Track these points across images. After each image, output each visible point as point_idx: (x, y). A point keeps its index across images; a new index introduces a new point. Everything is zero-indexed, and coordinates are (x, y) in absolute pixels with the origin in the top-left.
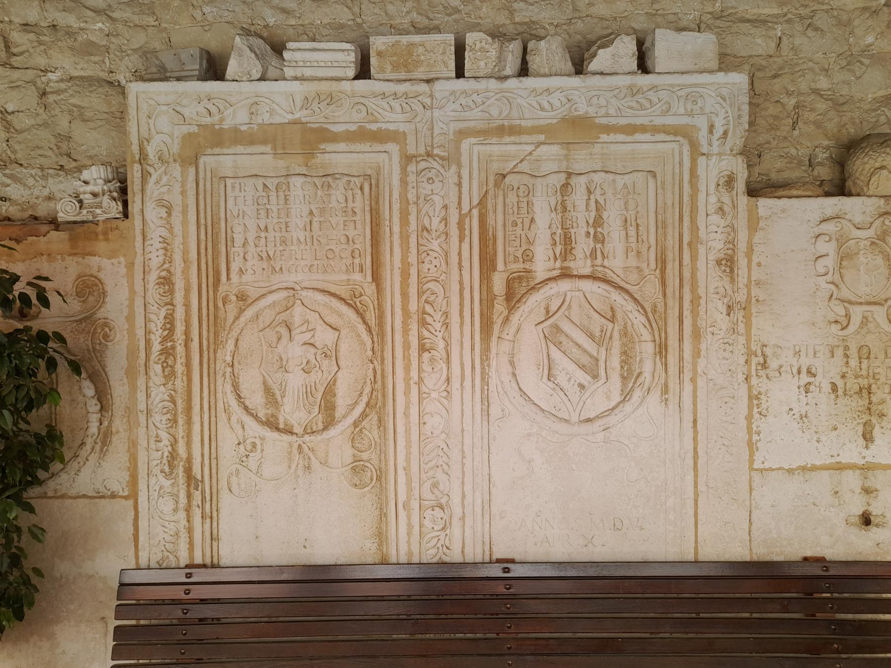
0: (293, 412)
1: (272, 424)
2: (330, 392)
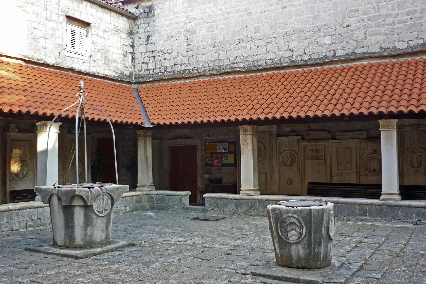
0: (415, 164)
1: (411, 166)
2: (421, 162)
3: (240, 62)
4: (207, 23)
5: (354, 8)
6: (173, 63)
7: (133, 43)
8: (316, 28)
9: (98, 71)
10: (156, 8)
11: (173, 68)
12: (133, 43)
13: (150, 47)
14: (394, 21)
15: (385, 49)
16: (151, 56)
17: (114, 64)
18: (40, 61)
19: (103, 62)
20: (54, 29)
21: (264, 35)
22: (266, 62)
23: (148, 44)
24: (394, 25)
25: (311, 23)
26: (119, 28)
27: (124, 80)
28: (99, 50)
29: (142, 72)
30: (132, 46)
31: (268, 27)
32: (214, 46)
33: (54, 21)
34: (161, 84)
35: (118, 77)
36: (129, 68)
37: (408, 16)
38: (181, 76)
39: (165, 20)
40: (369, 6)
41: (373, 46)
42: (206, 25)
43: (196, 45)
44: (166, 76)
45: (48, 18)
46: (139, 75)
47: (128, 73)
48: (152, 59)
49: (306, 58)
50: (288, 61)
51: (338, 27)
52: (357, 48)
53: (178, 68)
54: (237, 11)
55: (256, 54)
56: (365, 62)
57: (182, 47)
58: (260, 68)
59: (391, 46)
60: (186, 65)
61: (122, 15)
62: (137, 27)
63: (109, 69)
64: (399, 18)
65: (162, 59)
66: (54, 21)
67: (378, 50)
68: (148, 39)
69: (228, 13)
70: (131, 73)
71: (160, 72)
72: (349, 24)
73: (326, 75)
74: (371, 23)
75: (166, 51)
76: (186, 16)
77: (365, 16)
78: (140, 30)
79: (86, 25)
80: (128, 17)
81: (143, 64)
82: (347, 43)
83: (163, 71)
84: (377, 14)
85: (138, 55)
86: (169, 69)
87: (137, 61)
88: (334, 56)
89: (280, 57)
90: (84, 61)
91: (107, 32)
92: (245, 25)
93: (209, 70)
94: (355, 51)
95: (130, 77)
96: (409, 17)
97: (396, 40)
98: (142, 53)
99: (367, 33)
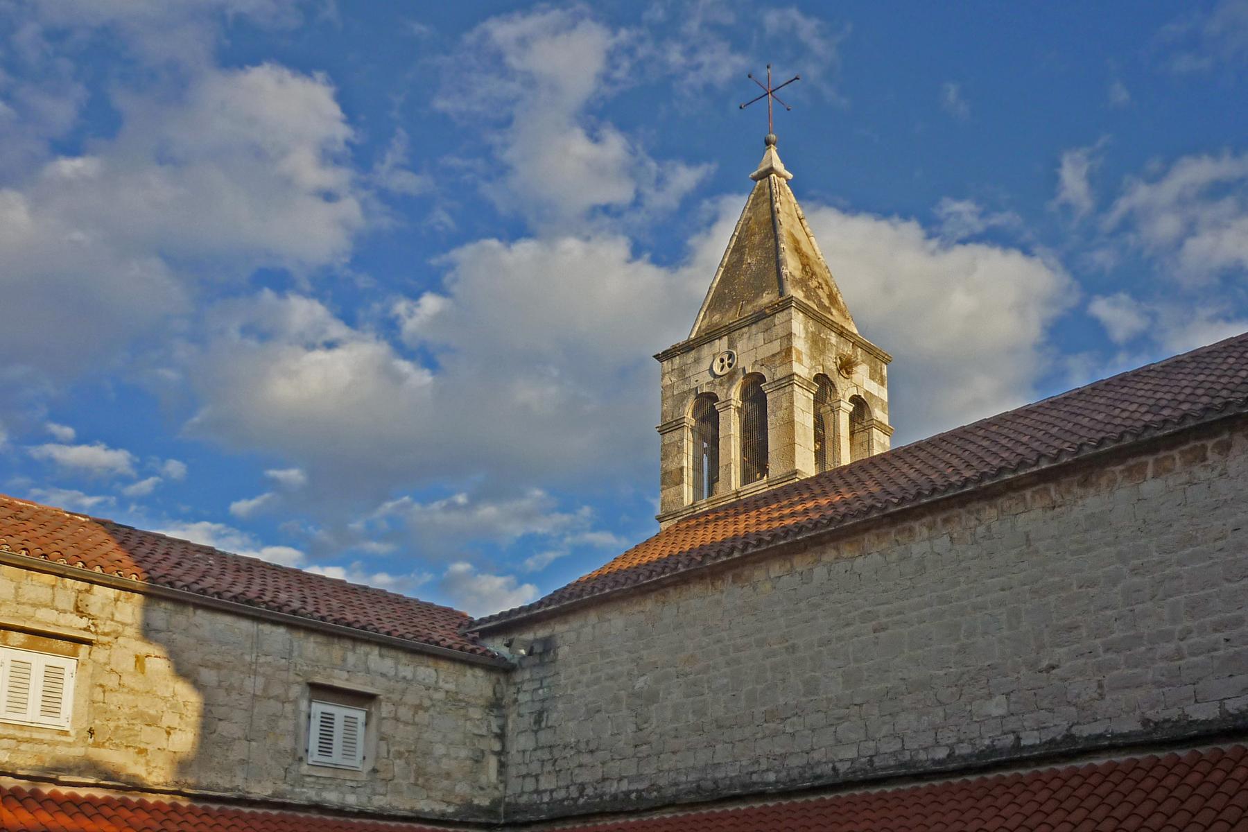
3: (768, 770)
4: (686, 675)
5: (1066, 621)
6: (599, 776)
7: (502, 727)
8: (966, 677)
9: (395, 804)
10: (559, 642)
11: (599, 786)
12: (502, 727)
13: (545, 737)
14: (1178, 650)
15: (1156, 724)
16: (545, 757)
17: (446, 783)
18: (228, 794)
19: (412, 781)
20: (274, 719)
21: (829, 700)
22: (834, 769)
23: (540, 729)
24: (1180, 659)
25: (951, 664)
26: (461, 697)
27: (471, 820)
28: (400, 755)
29: (524, 799)
30: (501, 736)
31: (840, 679)
32: (700, 729)
33: (277, 698)
34: (568, 827)
35: (456, 814)
36: (488, 791)
37: (1218, 635)
38: (618, 807)
39: (583, 672)
40: (1109, 613)
41: (1124, 716)
42: (681, 680)
43: (658, 731)
44: (583, 806)
45: (259, 693)
46: (517, 804)
47: (485, 802)
48: (548, 767)
49: (941, 754)
50: (892, 763)
51: (1024, 670)
52: (1078, 723)
53: (612, 788)
54: (760, 643)
55: (807, 747)
56: (1100, 761)
57: (623, 737)
58: (817, 783)
59: (1174, 714)
60: (631, 780)
61: (472, 665)
62: (513, 689)
63: (428, 797)
64: (1194, 639)
65: (572, 765)
66: (277, 698)
67: (1139, 727)
68: (539, 717)
69: (737, 649)
70: (496, 803)
71: (567, 799)
72: (1055, 663)
73: (1228, 774)
74: (1114, 656)
75: (582, 746)
76: (633, 661)
77: (1098, 641)
78: (523, 698)
79: (362, 699)
80: (489, 669)
81: (528, 780)
82: (1051, 711)
83: (575, 794)
84: (1132, 633)
85: (514, 756)
86: (589, 791)
87: (512, 771)
88: (1017, 746)
89: (870, 753)
90: (354, 784)
91: (426, 710)
92: (780, 676)
93: (690, 792)
94: (1074, 730)
95: (489, 811)
96: (1220, 636)
97: (1190, 698)
98: (524, 752)
99: (1105, 682)
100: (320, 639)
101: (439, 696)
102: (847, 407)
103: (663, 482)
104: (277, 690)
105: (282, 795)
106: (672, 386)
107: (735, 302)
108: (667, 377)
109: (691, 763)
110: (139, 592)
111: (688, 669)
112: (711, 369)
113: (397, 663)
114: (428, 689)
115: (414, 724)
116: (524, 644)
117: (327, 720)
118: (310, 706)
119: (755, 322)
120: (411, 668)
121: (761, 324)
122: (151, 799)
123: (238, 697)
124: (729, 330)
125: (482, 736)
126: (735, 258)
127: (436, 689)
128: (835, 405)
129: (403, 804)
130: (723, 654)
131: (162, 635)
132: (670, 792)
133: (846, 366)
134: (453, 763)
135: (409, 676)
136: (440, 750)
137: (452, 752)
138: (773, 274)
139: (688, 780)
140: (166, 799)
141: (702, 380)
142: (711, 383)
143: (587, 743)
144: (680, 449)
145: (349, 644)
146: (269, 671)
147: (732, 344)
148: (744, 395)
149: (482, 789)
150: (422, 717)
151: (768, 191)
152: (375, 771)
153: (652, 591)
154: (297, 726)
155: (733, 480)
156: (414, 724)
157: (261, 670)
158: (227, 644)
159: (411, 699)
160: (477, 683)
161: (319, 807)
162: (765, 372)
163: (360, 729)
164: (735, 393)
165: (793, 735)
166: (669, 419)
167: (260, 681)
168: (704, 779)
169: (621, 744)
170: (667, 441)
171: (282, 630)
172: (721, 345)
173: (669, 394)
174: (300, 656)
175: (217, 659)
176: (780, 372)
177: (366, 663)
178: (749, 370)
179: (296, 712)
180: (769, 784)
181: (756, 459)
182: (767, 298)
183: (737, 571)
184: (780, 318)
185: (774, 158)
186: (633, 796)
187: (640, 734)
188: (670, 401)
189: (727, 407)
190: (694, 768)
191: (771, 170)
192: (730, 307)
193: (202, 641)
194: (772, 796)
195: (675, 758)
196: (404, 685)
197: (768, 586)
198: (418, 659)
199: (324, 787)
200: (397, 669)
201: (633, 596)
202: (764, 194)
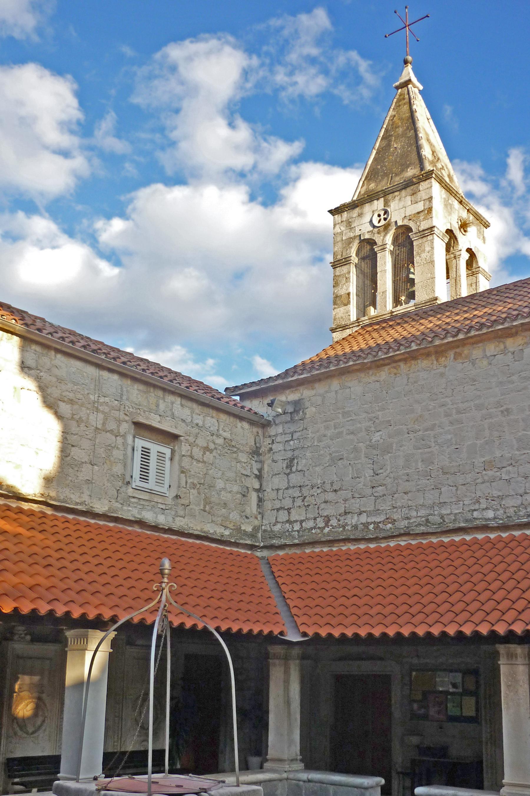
3: (487, 508)
4: (415, 432)
6: (342, 510)
7: (260, 470)
9: (191, 525)
10: (307, 404)
11: (342, 518)
12: (260, 470)
13: (295, 479)
18: (79, 507)
19: (202, 507)
20: (110, 448)
23: (291, 472)
26: (233, 443)
27: (241, 541)
28: (194, 486)
30: (259, 477)
33: (111, 432)
36: (251, 519)
39: (327, 428)
42: (412, 435)
44: (328, 534)
45: (99, 426)
47: (249, 529)
48: (299, 502)
54: (479, 407)
55: (521, 491)
57: (362, 479)
61: (241, 419)
63: (212, 521)
65: (319, 501)
66: (111, 432)
71: (315, 528)
75: (328, 487)
79: (172, 438)
80: (252, 423)
81: (281, 512)
85: (269, 494)
86: (334, 522)
87: (268, 505)
90: (163, 507)
91: (211, 451)
92: (496, 434)
98: (278, 490)
100: (142, 387)
101: (220, 441)
102: (465, 256)
103: (335, 303)
104: (111, 425)
105: (115, 511)
106: (341, 233)
107: (386, 175)
108: (338, 226)
109: (421, 502)
110: (17, 335)
111: (417, 427)
112: (371, 222)
113: (192, 412)
114: (212, 435)
115: (204, 462)
116: (283, 404)
117: (146, 452)
118: (134, 441)
119: (405, 188)
120: (201, 417)
121: (408, 190)
122: (26, 506)
123: (85, 428)
124: (385, 194)
125: (247, 476)
126: (385, 143)
127: (218, 436)
128: (458, 253)
129: (196, 526)
130: (447, 415)
131: (32, 372)
132: (403, 524)
133: (464, 226)
134: (229, 495)
135: (201, 424)
136: (220, 484)
137: (228, 486)
138: (414, 156)
139: (417, 516)
140: (35, 507)
141: (363, 228)
142: (372, 231)
143: (332, 484)
144: (348, 279)
145: (160, 393)
146: (107, 409)
147: (386, 204)
148: (395, 240)
149: (247, 518)
150: (209, 457)
151: (407, 96)
152: (177, 497)
153: (385, 365)
154: (125, 455)
155: (386, 303)
156: (204, 462)
157: (101, 408)
158: (78, 384)
159: (201, 442)
160: (244, 433)
161: (141, 523)
162: (411, 224)
163: (168, 463)
164: (389, 239)
165: (508, 481)
166: (339, 257)
167: (101, 416)
168: (431, 515)
169: (360, 486)
170: (338, 273)
171: (116, 377)
172: (379, 204)
173: (339, 239)
174: (127, 399)
175: (71, 395)
176: (424, 225)
177: (171, 410)
178: (400, 223)
179: (125, 444)
180: (489, 519)
181: (404, 286)
182: (411, 172)
183: (458, 350)
184: (423, 186)
185: (409, 73)
186: (371, 527)
187: (377, 477)
188: (340, 244)
189: (384, 249)
190: (423, 505)
191: (409, 81)
192: (383, 179)
193: (60, 380)
194: (493, 529)
195: (406, 497)
196: (197, 431)
197: (485, 362)
198: (206, 410)
199: (143, 508)
200: (192, 417)
201: (370, 368)
202: (404, 99)
